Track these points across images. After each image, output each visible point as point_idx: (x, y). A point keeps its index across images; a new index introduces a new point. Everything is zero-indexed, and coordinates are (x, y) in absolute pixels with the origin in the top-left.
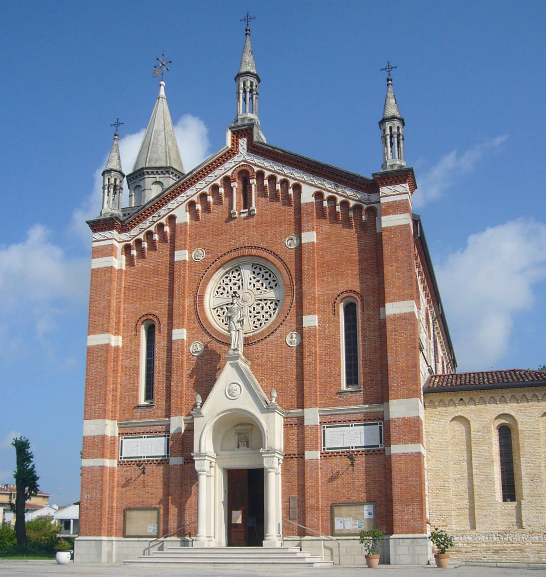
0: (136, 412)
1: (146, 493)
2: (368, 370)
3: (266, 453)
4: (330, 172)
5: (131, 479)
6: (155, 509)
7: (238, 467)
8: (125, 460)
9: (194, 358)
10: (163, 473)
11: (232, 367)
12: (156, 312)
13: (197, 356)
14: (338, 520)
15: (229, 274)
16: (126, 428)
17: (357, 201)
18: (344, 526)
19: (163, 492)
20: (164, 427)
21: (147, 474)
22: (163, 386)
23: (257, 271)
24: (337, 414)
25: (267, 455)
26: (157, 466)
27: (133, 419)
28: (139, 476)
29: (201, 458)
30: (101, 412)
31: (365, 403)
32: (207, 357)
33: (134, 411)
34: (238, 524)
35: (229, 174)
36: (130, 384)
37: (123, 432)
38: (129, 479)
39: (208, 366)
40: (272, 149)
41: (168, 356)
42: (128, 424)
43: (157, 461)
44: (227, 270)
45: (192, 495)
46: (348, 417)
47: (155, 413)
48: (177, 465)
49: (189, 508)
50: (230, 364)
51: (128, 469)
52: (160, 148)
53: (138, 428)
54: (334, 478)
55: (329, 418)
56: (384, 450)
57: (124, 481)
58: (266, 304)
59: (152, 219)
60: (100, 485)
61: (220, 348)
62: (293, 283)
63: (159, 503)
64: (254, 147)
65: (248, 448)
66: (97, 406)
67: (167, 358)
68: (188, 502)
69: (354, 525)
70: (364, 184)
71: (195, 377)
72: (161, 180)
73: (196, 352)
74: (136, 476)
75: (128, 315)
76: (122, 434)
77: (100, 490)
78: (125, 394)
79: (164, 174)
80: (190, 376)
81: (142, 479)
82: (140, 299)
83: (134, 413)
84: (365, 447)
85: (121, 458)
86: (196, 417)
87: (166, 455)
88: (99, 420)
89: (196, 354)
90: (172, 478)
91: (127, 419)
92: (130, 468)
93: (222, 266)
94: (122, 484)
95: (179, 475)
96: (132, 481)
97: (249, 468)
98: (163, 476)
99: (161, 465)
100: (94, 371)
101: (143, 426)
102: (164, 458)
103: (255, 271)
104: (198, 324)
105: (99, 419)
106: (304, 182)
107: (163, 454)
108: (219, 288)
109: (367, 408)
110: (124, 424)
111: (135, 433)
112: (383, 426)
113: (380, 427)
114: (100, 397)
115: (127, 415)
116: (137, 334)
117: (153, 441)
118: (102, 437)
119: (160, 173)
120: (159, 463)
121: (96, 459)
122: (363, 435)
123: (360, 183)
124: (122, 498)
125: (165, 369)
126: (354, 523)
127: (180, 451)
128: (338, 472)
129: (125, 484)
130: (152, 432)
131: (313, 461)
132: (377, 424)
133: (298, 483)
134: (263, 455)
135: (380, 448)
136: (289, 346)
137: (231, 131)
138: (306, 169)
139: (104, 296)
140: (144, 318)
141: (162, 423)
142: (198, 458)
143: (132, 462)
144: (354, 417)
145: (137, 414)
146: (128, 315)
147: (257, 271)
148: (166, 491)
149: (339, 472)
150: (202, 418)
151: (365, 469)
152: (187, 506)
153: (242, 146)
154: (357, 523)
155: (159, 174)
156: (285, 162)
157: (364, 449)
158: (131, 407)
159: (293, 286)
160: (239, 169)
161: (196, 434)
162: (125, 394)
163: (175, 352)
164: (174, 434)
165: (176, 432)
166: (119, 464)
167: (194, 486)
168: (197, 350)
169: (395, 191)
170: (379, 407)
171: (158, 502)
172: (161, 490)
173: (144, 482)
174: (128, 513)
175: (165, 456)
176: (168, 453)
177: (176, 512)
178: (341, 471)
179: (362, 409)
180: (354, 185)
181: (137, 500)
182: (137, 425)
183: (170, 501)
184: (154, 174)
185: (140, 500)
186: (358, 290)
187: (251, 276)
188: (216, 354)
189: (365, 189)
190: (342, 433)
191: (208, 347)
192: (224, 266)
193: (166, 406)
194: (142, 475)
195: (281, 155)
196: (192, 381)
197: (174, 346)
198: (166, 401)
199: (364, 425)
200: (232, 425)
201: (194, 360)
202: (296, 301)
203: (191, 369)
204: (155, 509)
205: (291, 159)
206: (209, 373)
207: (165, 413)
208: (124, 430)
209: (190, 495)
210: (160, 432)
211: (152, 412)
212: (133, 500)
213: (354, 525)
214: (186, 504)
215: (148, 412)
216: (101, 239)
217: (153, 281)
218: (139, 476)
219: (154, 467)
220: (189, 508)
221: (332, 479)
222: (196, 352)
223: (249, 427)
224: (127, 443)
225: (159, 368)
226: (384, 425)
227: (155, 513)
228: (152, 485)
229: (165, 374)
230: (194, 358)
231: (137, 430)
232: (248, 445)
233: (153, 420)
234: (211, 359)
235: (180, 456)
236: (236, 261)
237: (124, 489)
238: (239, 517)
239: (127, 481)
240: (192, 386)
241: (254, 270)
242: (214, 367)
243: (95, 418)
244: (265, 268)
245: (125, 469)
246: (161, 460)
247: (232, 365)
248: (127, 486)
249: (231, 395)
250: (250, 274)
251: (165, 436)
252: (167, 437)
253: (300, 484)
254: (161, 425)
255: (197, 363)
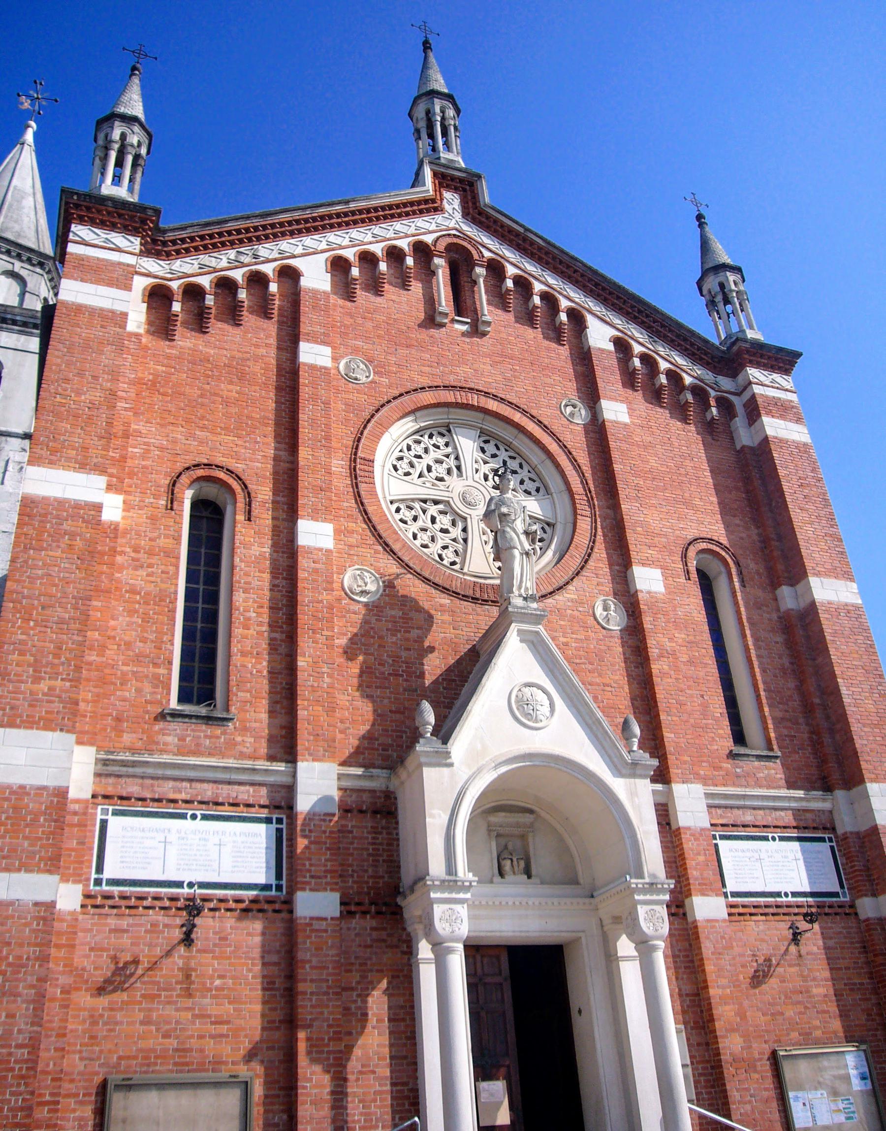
0: (162, 732)
1: (195, 1016)
2: (779, 714)
3: (644, 891)
4: (640, 312)
5: (136, 962)
6: (232, 1082)
7: (510, 934)
8: (116, 890)
9: (356, 607)
10: (263, 946)
11: (522, 641)
12: (238, 467)
13: (366, 605)
14: (796, 1098)
15: (422, 436)
16: (123, 780)
17: (696, 378)
18: (814, 1117)
19: (263, 1015)
20: (264, 791)
21: (199, 944)
22: (259, 667)
23: (490, 448)
24: (738, 808)
25: (648, 897)
26: (239, 919)
27: (151, 752)
28: (168, 953)
29: (454, 895)
30: (57, 706)
31: (791, 786)
32: (393, 613)
33: (157, 727)
34: (501, 1127)
35: (429, 239)
36: (144, 640)
37: (110, 790)
38: (126, 964)
39: (399, 635)
40: (521, 230)
41: (274, 586)
42: (134, 764)
43: (238, 901)
44: (423, 424)
45: (369, 1025)
46: (760, 817)
47: (232, 744)
48: (325, 919)
49: (361, 1072)
50: (519, 630)
51: (124, 923)
52: (26, 219)
53: (171, 784)
54: (764, 976)
55: (730, 817)
56: (852, 906)
57: (107, 970)
58: (454, 540)
59: (236, 257)
60: (32, 980)
61: (431, 598)
62: (590, 492)
63: (250, 1056)
64: (480, 214)
65: (529, 877)
66: (44, 686)
67: (271, 590)
68: (357, 1052)
69: (835, 1111)
70: (706, 354)
71: (361, 658)
72: (24, 273)
73: (363, 593)
74: (158, 951)
75: (147, 451)
76: (106, 797)
77: (28, 1002)
78: (125, 668)
79: (33, 265)
80: (345, 652)
81: (180, 963)
82: (187, 421)
83: (158, 733)
84: (813, 894)
85: (98, 882)
86: (430, 765)
87: (273, 882)
88: (49, 734)
89: (364, 599)
90: (309, 961)
91: (133, 750)
92: (131, 920)
93: (413, 412)
94: (99, 977)
95: (331, 953)
96: (140, 972)
97: (509, 944)
98: (263, 957)
99: (255, 918)
100: (40, 572)
101: (191, 780)
102: (268, 893)
103: (486, 446)
104: (365, 526)
105: (46, 728)
106: (590, 312)
107: (261, 879)
108: (401, 459)
109: (800, 798)
110: (124, 764)
111: (159, 800)
112: (838, 846)
113: (271, 885)
114: (57, 656)
115: (127, 738)
116: (175, 507)
117: (223, 833)
118: (57, 795)
119: (24, 258)
120: (246, 910)
121: (23, 876)
122: (801, 863)
123: (699, 349)
124: (92, 1037)
125: (265, 619)
126: (833, 1107)
127: (330, 871)
128: (768, 960)
129: (107, 981)
130: (222, 804)
131: (717, 925)
132: (822, 840)
133: (680, 990)
134: (636, 897)
135: (842, 899)
136: (604, 628)
137: (431, 170)
138: (591, 291)
139: (95, 378)
140: (200, 472)
141: (258, 778)
142: (446, 895)
143: (141, 898)
144: (771, 818)
145: (169, 739)
146: (147, 451)
147: (490, 448)
148: (271, 1009)
149: (770, 960)
150: (445, 770)
151: (826, 954)
152: (354, 1065)
153: (450, 203)
154: (841, 1106)
155: (22, 261)
156: (547, 263)
157: (810, 899)
158: (147, 712)
159: (592, 499)
160: (450, 240)
161: (433, 816)
162: (125, 668)
163: (306, 579)
164: (311, 816)
165: (317, 810)
166: (89, 902)
167: (375, 993)
168: (364, 588)
169: (773, 381)
170: (824, 800)
171: (242, 1052)
172: (258, 1007)
173: (188, 976)
174: (118, 1102)
175: (266, 887)
176: (279, 876)
177: (328, 1090)
178: (775, 955)
179: (790, 799)
180: (686, 349)
181: (155, 1042)
182: (169, 772)
183: (302, 1047)
184: (12, 257)
185: (173, 1043)
186: (724, 541)
187: (479, 455)
188: (419, 609)
189: (708, 364)
190: (756, 856)
191: (394, 587)
192: (418, 414)
193: (270, 725)
194: (182, 949)
195: (540, 248)
196: (354, 669)
197: (304, 563)
198: (270, 712)
199: (799, 839)
200: (480, 810)
201: (355, 613)
202: (603, 532)
203: (349, 636)
204: (232, 1082)
205: (561, 262)
206: (404, 654)
207: (269, 748)
208: (115, 785)
209: (364, 1027)
210: (248, 806)
211: (222, 740)
212: (141, 1044)
213: (835, 1111)
214: (348, 1059)
215: (206, 737)
216: (96, 242)
217: (229, 390)
218: (168, 953)
219: (230, 922)
220: (361, 1072)
221: (758, 978)
222: (363, 593)
223: (527, 818)
224: (124, 828)
225: (248, 614)
226: (837, 842)
227: (231, 1099)
228: (218, 989)
229: (266, 634)
230: (356, 607)
231: (167, 789)
232: (528, 873)
233: (231, 762)
234: (406, 618)
235: (332, 890)
236: (443, 413)
237: (103, 1001)
238: (502, 1102)
239: (118, 971)
240: (355, 681)
241: (482, 445)
242: (415, 641)
243: (30, 723)
244: (509, 446)
245: (112, 922)
246: (254, 901)
247: (525, 637)
248: (119, 987)
249: (527, 715)
250: (475, 453)
251: (268, 821)
252: (274, 826)
253: (684, 993)
254: (252, 784)
255: (365, 622)
